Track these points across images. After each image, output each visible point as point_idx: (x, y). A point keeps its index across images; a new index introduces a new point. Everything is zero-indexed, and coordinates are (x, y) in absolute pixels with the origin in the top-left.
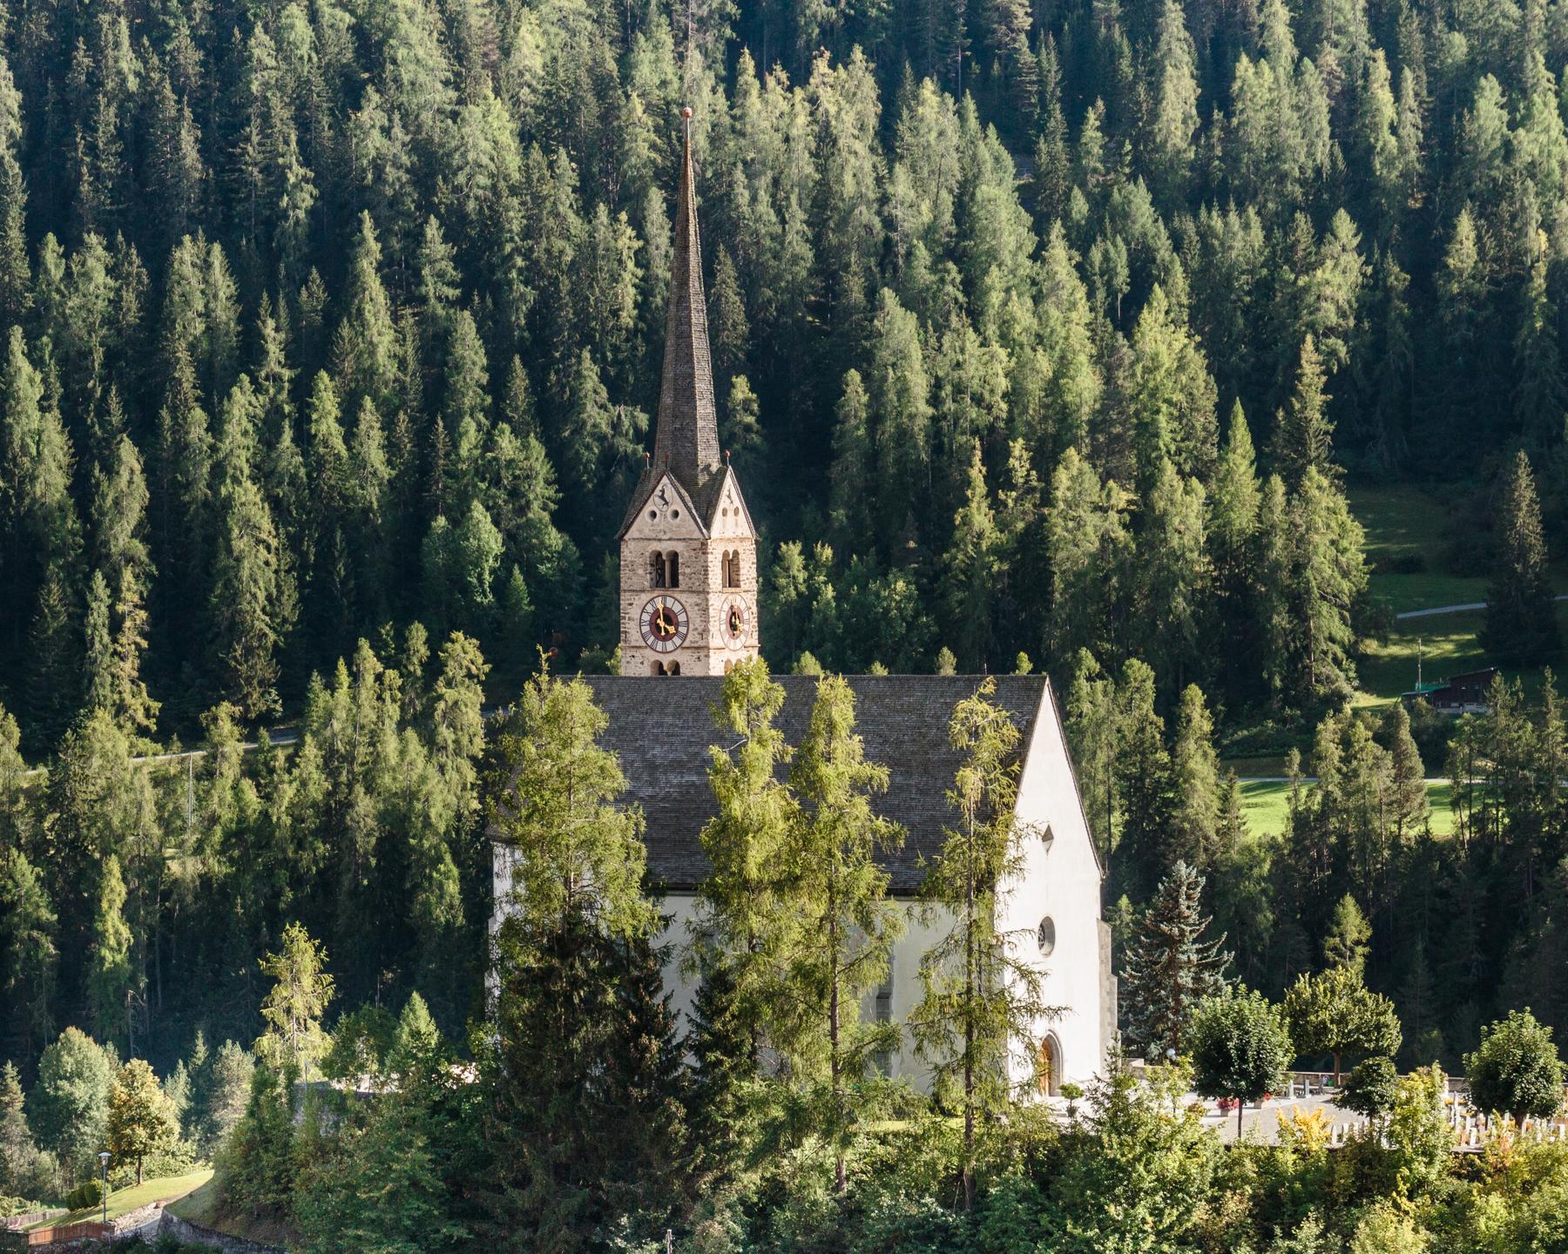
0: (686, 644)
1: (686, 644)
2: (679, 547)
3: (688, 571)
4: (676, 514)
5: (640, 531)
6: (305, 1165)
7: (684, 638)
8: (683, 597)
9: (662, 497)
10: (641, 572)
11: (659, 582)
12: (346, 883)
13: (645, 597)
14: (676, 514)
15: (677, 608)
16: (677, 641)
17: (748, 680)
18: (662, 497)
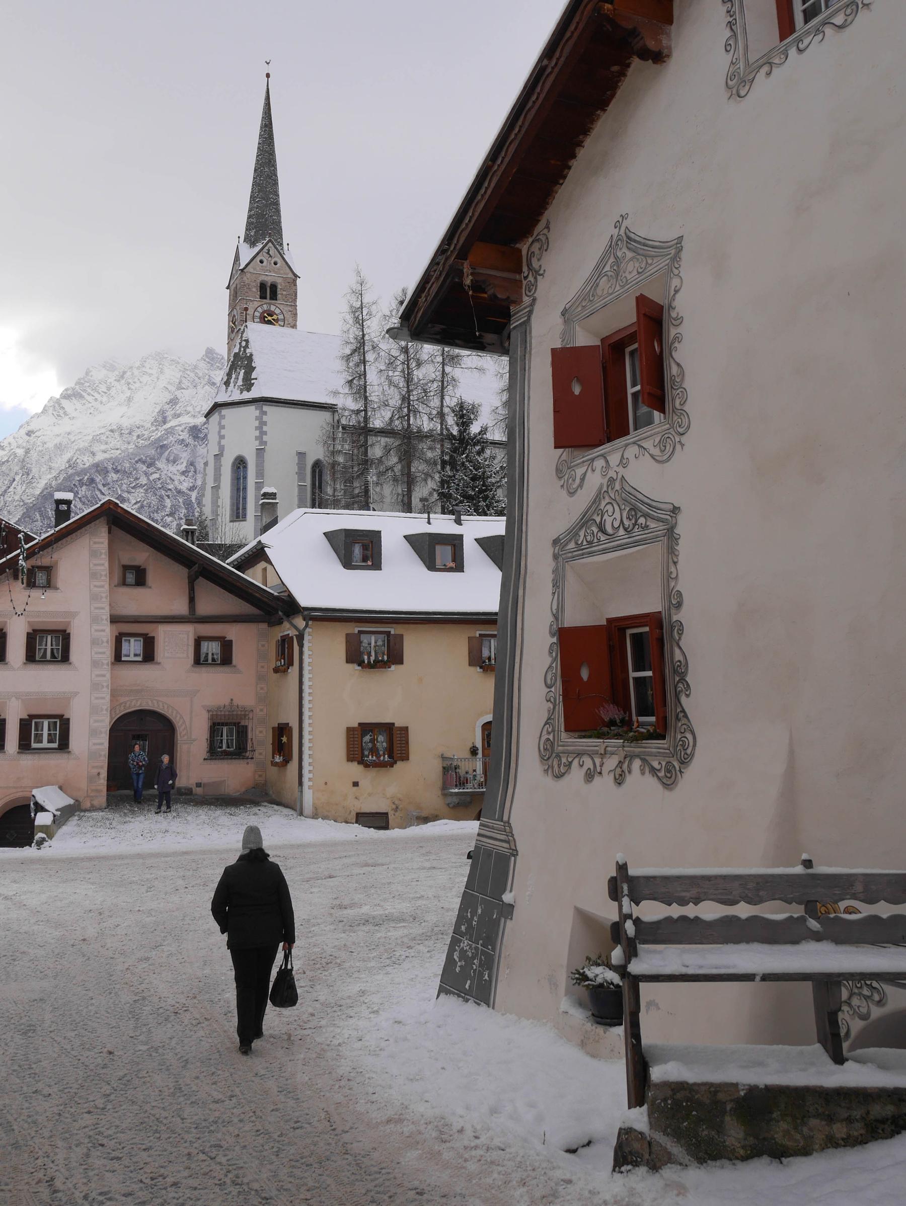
2: (279, 281)
8: (281, 307)
9: (268, 253)
10: (254, 290)
18: (268, 253)
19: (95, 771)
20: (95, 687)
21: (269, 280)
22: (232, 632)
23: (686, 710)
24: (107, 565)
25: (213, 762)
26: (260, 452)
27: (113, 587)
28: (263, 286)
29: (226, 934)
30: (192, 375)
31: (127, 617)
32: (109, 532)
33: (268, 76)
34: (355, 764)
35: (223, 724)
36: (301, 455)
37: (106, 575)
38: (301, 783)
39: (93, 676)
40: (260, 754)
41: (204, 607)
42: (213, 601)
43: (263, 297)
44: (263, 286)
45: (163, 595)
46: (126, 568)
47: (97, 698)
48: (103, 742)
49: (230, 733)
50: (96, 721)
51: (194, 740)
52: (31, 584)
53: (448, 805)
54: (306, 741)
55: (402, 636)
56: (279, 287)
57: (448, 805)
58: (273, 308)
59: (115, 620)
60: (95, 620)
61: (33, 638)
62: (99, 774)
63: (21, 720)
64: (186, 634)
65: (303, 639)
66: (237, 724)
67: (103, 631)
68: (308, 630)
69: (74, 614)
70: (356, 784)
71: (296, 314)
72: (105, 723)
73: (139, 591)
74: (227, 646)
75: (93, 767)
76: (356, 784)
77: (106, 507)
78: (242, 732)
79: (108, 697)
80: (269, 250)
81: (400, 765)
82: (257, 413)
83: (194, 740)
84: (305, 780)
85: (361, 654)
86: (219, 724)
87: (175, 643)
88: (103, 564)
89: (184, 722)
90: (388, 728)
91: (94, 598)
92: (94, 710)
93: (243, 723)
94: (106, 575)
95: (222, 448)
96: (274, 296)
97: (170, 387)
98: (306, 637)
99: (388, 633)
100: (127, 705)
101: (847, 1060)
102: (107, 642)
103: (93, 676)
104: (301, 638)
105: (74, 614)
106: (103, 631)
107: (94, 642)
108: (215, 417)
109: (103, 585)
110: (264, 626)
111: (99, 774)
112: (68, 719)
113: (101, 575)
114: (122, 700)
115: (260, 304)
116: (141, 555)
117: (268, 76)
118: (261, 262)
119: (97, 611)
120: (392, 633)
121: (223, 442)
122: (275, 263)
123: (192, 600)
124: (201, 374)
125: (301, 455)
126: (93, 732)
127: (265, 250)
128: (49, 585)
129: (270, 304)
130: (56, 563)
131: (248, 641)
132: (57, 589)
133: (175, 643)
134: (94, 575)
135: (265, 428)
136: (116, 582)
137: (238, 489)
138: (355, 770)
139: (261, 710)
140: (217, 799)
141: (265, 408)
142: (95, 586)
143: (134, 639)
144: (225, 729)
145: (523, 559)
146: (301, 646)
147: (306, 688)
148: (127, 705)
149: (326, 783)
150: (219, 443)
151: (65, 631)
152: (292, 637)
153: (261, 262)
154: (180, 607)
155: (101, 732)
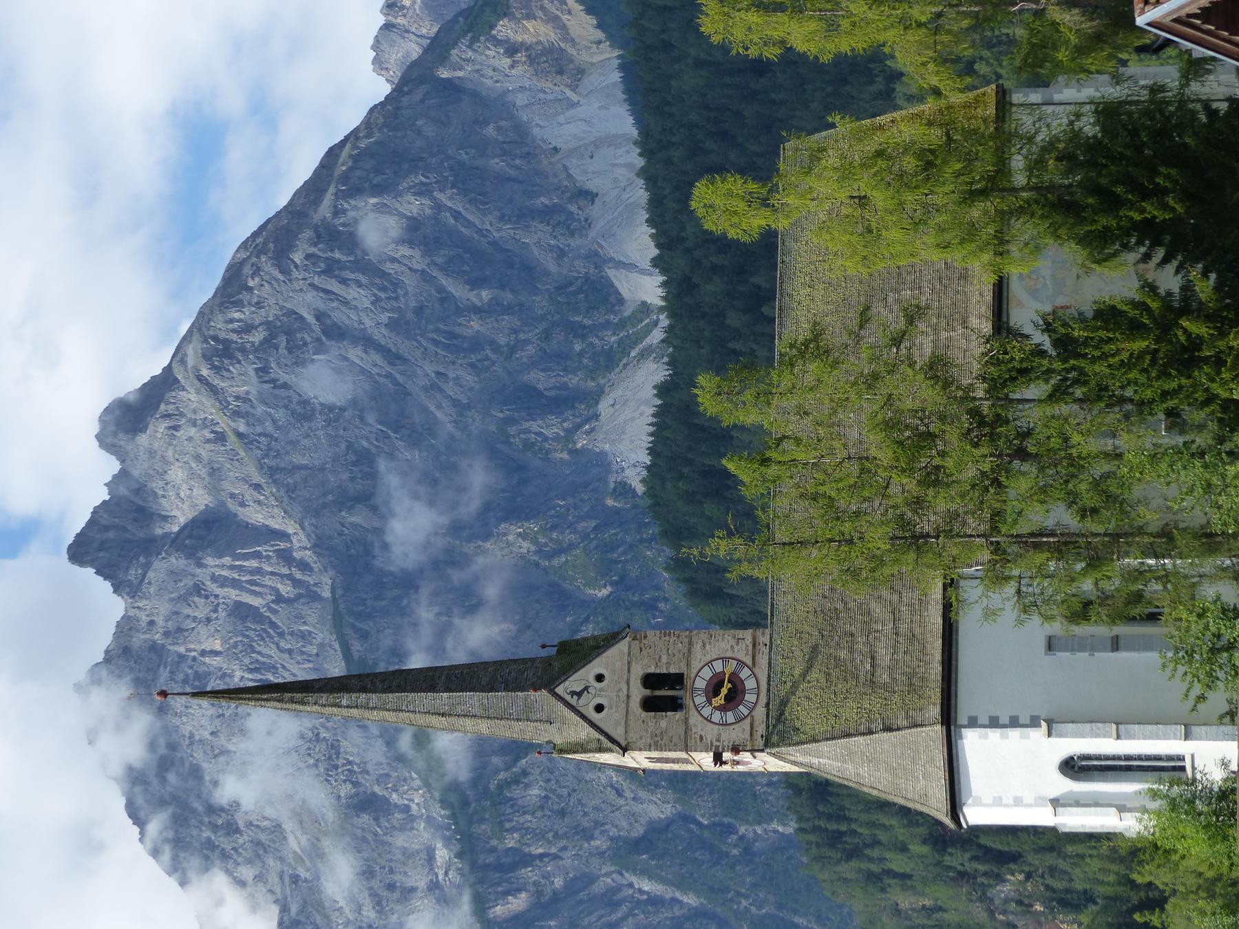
0: (749, 661)
1: (749, 661)
2: (638, 671)
3: (664, 659)
4: (600, 678)
5: (617, 724)
6: (1221, 895)
7: (741, 664)
8: (696, 665)
9: (579, 694)
10: (663, 724)
11: (674, 705)
12: (1147, 322)
13: (694, 718)
14: (600, 678)
15: (707, 674)
16: (744, 674)
17: (1001, 254)
18: (579, 694)
23: (1014, 733)
36: (1051, 645)
44: (650, 705)
56: (652, 670)
58: (701, 684)
80: (573, 693)
96: (677, 680)
115: (693, 712)
118: (599, 708)
121: (1029, 799)
125: (1051, 645)
127: (573, 701)
129: (693, 690)
137: (1129, 768)
140: (951, 625)
145: (1005, 302)
153: (599, 708)
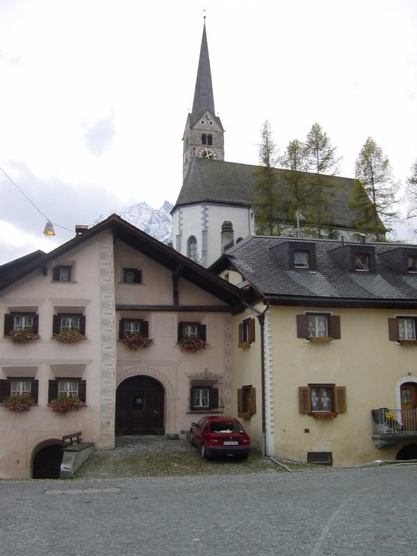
19: (105, 421)
20: (105, 356)
21: (207, 133)
22: (207, 320)
24: (112, 264)
25: (193, 415)
26: (205, 232)
27: (117, 284)
28: (204, 137)
29: (54, 379)
30: (157, 216)
31: (127, 306)
32: (114, 243)
33: (205, 17)
34: (307, 416)
35: (200, 388)
37: (112, 272)
38: (264, 430)
39: (103, 365)
40: (228, 409)
41: (185, 301)
42: (191, 297)
43: (204, 143)
45: (154, 290)
46: (126, 271)
47: (106, 365)
48: (112, 398)
49: (205, 395)
50: (106, 382)
51: (179, 399)
52: (56, 278)
53: (377, 446)
54: (267, 397)
55: (339, 317)
56: (213, 137)
57: (377, 446)
59: (119, 308)
60: (104, 305)
61: (59, 319)
62: (109, 423)
63: (50, 381)
64: (172, 320)
65: (264, 319)
66: (210, 388)
67: (110, 314)
68: (268, 312)
69: (89, 301)
70: (307, 431)
71: (223, 153)
72: (113, 385)
73: (136, 287)
74: (202, 330)
75: (105, 417)
76: (307, 431)
77: (112, 219)
78: (214, 394)
79: (115, 364)
81: (340, 417)
82: (203, 209)
83: (179, 399)
84: (268, 427)
85: (309, 333)
86: (197, 387)
87: (163, 329)
88: (110, 261)
89: (171, 385)
90: (330, 388)
91: (103, 289)
92: (104, 374)
93: (215, 387)
94: (112, 272)
95: (181, 231)
96: (210, 143)
97: (145, 223)
98: (266, 322)
99: (328, 315)
100: (129, 371)
101: (116, 446)
102: (114, 339)
103: (103, 365)
104: (261, 318)
105: (89, 301)
106: (110, 314)
107: (104, 323)
108: (177, 213)
109: (110, 279)
110: (229, 315)
111: (109, 423)
112: (85, 381)
113: (108, 272)
114: (126, 368)
116: (137, 260)
117: (205, 17)
118: (203, 122)
119: (107, 367)
120: (332, 315)
122: (211, 123)
123: (176, 294)
124: (162, 216)
126: (104, 391)
128: (69, 279)
130: (74, 262)
131: (217, 327)
132: (75, 282)
133: (163, 329)
134: (103, 272)
135: (207, 219)
136: (119, 281)
138: (308, 421)
139: (228, 377)
141: (207, 207)
142: (104, 280)
143: (133, 332)
144: (201, 391)
146: (262, 324)
147: (267, 356)
148: (129, 371)
149: (284, 431)
150: (180, 228)
151: (82, 314)
152: (254, 319)
153: (203, 122)
154: (168, 300)
155: (110, 391)
